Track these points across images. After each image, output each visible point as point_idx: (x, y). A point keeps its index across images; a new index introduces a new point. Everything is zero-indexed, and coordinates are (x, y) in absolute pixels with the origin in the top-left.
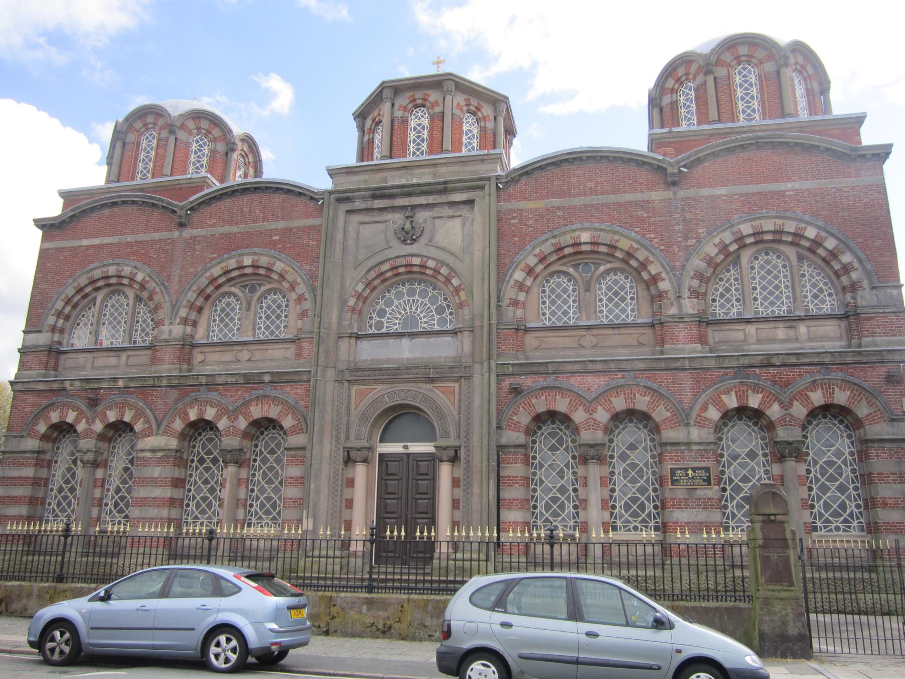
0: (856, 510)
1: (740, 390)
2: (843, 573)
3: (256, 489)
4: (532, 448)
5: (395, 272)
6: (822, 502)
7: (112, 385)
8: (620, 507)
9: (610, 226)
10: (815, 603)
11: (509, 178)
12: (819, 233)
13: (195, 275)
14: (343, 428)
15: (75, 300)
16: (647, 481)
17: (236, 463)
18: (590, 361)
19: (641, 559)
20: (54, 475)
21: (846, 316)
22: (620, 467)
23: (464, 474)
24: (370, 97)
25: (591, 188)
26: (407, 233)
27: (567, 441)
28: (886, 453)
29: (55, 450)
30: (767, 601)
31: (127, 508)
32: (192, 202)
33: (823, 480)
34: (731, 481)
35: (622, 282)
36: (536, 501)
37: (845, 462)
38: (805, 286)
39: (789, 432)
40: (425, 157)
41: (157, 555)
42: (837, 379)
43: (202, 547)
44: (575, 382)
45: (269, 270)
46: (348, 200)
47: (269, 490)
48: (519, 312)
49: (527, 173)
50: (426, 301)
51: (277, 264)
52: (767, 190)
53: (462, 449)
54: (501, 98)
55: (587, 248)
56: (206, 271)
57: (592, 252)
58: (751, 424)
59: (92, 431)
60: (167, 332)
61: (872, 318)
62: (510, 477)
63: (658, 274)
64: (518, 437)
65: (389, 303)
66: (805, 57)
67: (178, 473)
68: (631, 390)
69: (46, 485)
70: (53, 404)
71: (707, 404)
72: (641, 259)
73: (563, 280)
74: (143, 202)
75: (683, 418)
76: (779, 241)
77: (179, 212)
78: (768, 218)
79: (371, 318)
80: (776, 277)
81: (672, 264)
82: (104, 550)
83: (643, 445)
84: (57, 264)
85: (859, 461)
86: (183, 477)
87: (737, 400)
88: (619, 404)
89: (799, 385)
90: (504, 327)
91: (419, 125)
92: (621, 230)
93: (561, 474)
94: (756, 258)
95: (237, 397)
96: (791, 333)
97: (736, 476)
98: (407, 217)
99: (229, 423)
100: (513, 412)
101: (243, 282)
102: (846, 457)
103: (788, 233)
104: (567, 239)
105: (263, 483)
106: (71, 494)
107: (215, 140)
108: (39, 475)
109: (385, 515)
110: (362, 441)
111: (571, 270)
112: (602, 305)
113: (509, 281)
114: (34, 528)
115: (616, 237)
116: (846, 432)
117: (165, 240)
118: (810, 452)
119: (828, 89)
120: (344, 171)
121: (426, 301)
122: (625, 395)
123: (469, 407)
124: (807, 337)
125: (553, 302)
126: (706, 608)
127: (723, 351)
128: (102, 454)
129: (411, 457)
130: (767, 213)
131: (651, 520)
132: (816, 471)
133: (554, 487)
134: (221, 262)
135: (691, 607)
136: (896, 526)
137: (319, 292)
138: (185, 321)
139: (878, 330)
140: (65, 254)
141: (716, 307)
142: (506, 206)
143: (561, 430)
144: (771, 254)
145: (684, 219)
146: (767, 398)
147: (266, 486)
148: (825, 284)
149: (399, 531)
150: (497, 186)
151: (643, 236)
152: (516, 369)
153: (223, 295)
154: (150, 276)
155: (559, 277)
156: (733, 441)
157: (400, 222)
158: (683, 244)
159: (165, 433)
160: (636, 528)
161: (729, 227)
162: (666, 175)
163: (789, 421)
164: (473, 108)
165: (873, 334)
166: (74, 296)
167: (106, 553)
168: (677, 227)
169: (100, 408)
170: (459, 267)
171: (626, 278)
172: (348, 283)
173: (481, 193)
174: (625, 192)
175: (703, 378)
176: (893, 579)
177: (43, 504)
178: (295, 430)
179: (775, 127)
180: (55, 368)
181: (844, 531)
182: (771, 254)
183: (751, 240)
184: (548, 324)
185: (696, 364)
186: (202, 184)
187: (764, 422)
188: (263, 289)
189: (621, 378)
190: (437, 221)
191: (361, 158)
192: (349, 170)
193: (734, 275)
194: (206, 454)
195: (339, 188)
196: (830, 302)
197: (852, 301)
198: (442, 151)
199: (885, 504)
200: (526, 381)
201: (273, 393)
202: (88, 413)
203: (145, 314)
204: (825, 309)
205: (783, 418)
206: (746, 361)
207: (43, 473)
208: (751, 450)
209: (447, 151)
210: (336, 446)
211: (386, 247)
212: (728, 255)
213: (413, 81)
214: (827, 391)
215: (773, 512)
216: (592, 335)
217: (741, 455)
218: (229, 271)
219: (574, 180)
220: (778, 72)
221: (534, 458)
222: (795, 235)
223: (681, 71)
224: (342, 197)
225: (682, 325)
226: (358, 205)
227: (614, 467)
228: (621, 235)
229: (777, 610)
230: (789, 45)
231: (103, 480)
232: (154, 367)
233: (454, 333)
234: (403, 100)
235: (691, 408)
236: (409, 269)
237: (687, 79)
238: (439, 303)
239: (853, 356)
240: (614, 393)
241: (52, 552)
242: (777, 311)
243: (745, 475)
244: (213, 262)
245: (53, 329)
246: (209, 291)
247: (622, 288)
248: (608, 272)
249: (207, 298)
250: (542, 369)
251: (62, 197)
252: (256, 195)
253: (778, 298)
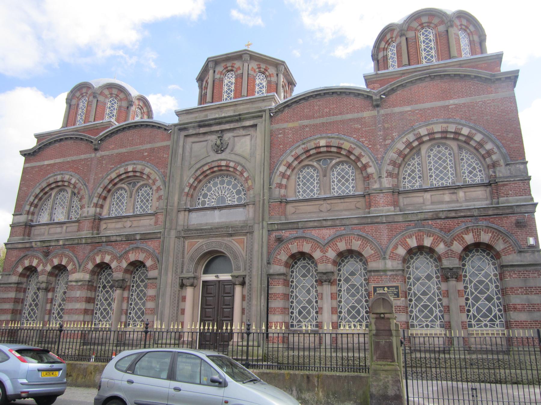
0: (498, 313)
1: (418, 236)
2: (494, 355)
3: (133, 303)
4: (291, 276)
5: (212, 171)
6: (475, 307)
7: (56, 243)
8: (345, 312)
9: (337, 135)
10: (467, 375)
11: (277, 110)
12: (471, 131)
13: (102, 178)
14: (180, 265)
15: (40, 196)
16: (361, 296)
17: (121, 287)
18: (324, 220)
19: (356, 346)
20: (27, 297)
21: (489, 185)
22: (345, 287)
23: (248, 293)
24: (203, 68)
25: (327, 112)
26: (218, 147)
27: (312, 271)
28: (516, 274)
29: (29, 282)
30: (376, 372)
31: (143, 316)
32: (101, 136)
33: (476, 293)
34: (415, 294)
35: (339, 170)
36: (293, 309)
37: (491, 281)
38: (463, 166)
39: (450, 261)
40: (232, 100)
41: (77, 343)
42: (482, 226)
43: (102, 339)
44: (315, 233)
45: (142, 173)
46: (185, 129)
47: (140, 304)
48: (283, 191)
49: (288, 106)
50: (230, 187)
51: (146, 170)
52: (437, 106)
53: (247, 277)
54: (280, 63)
55: (325, 149)
56: (108, 175)
57: (328, 152)
58: (428, 257)
59: (45, 271)
60: (86, 212)
61: (504, 185)
62: (275, 294)
63: (367, 163)
64: (281, 269)
65: (209, 190)
66: (468, 20)
67: (90, 294)
68: (349, 237)
69: (22, 302)
70: (26, 255)
71: (397, 245)
72: (357, 154)
73: (311, 170)
74: (76, 138)
75: (381, 255)
76: (446, 138)
77: (95, 142)
78: (437, 123)
79: (199, 199)
80: (444, 161)
81: (376, 156)
82: (51, 340)
83: (359, 272)
84: (31, 176)
85: (500, 280)
86: (93, 297)
87: (417, 242)
88: (342, 246)
89: (458, 230)
90: (273, 201)
91: (229, 82)
92: (345, 137)
93: (308, 292)
94: (432, 150)
95: (122, 249)
96: (454, 197)
97: (418, 291)
98: (219, 137)
99: (117, 264)
100: (277, 253)
101: (129, 181)
102: (492, 278)
103: (451, 132)
104: (312, 145)
105: (137, 300)
106: (358, 304)
107: (121, 100)
108: (18, 296)
109: (223, 319)
110: (190, 273)
111: (315, 164)
112: (334, 185)
113: (276, 172)
114: (17, 325)
115: (341, 142)
116: (491, 261)
117: (87, 159)
118: (467, 275)
119: (485, 40)
120: (184, 112)
121: (230, 187)
122: (345, 240)
123: (251, 250)
124: (464, 199)
125: (304, 184)
126: (339, 376)
127: (409, 210)
128: (51, 284)
129: (221, 283)
130: (437, 120)
131: (475, 322)
132: (471, 287)
133: (304, 300)
134: (116, 170)
135: (331, 376)
136: (523, 324)
137: (167, 185)
138: (96, 205)
139: (510, 192)
140: (36, 170)
141: (405, 182)
142: (276, 126)
143: (309, 264)
144: (441, 146)
145: (384, 128)
146: (436, 240)
147: (138, 301)
148: (477, 164)
149: (213, 326)
150: (270, 115)
151: (358, 140)
152: (279, 226)
153: (118, 189)
154: (78, 180)
155: (308, 169)
156: (417, 269)
157: (215, 141)
158: (383, 143)
159: (83, 271)
160: (427, 326)
161: (412, 131)
162: (372, 101)
163: (451, 255)
164: (262, 70)
165: (507, 195)
166: (39, 193)
167: (52, 342)
168: (379, 133)
169: (50, 257)
170: (248, 165)
171: (349, 167)
172: (185, 178)
173: (261, 120)
174: (347, 113)
175: (395, 228)
176: (520, 360)
177: (20, 313)
178: (154, 267)
179: (443, 65)
180: (29, 235)
181: (490, 327)
182: (441, 146)
183: (427, 138)
184: (301, 198)
185: (390, 219)
186: (110, 124)
187: (435, 256)
188: (139, 184)
189: (343, 230)
190: (236, 139)
191: (200, 102)
192: (187, 111)
193: (417, 161)
194: (107, 283)
195: (182, 122)
196: (480, 175)
197: (493, 174)
198: (241, 96)
199: (515, 309)
200: (286, 234)
201: (141, 246)
202: (44, 260)
203: (77, 202)
204: (477, 181)
205: (446, 253)
206: (422, 216)
207: (21, 296)
208: (428, 275)
209: (244, 96)
210: (175, 277)
211: (207, 155)
212: (412, 149)
213: (225, 56)
214: (476, 234)
215: (383, 311)
216: (328, 204)
217: (422, 278)
218: (121, 175)
219: (316, 108)
220: (447, 31)
221: (292, 282)
222: (455, 133)
223: (388, 36)
224: (182, 128)
225: (382, 195)
226: (191, 132)
227: (341, 287)
228: (345, 140)
229: (382, 378)
230: (454, 13)
231: (52, 299)
232: (79, 232)
233: (244, 206)
234: (219, 69)
235: (387, 248)
236: (220, 168)
237: (392, 41)
238: (238, 188)
239: (493, 210)
240: (339, 240)
241: (23, 341)
242: (445, 183)
243: (424, 291)
244: (112, 170)
245: (28, 213)
246: (109, 187)
247: (347, 173)
248: (338, 164)
249: (109, 191)
250: (295, 226)
251: (36, 138)
252: (136, 130)
253: (446, 175)
